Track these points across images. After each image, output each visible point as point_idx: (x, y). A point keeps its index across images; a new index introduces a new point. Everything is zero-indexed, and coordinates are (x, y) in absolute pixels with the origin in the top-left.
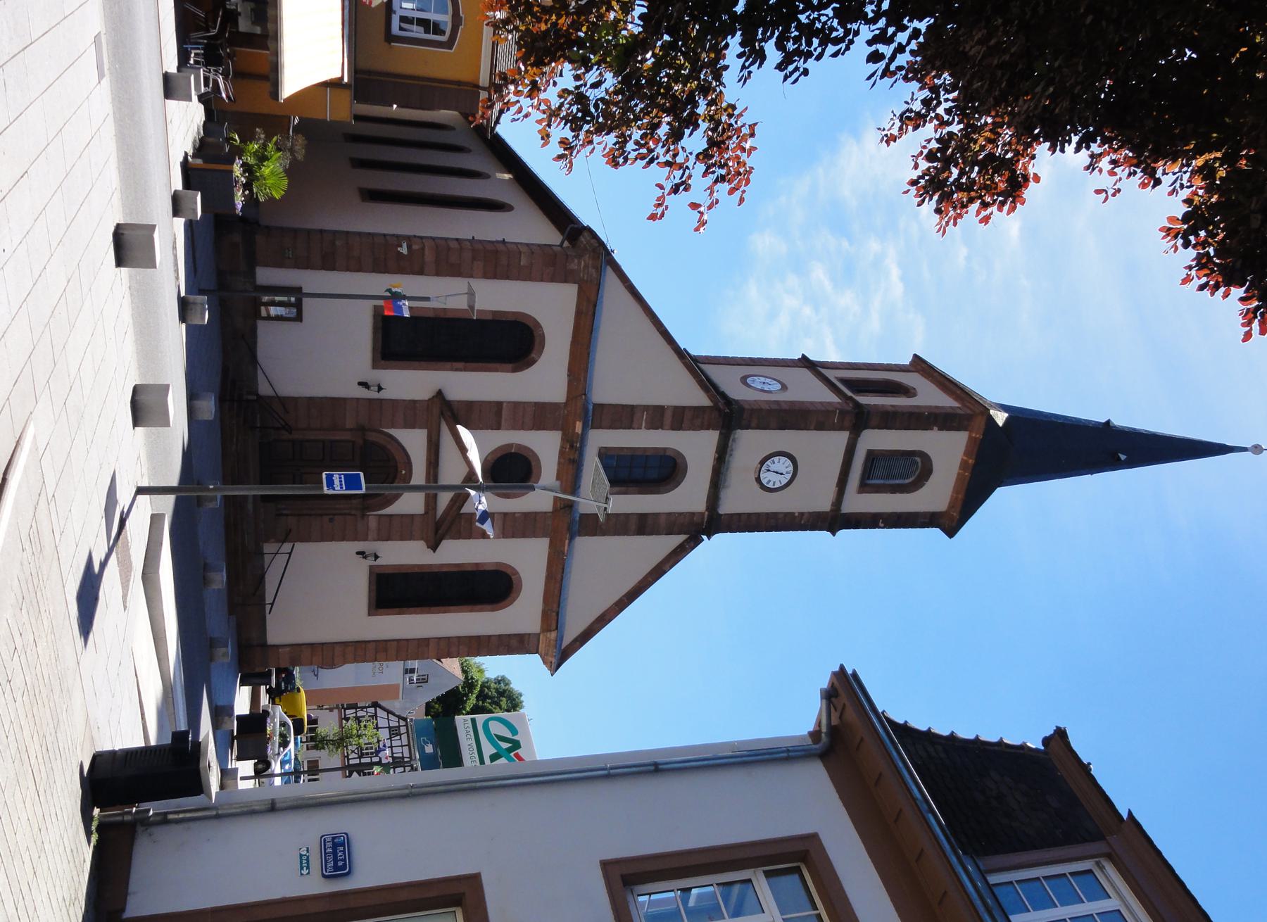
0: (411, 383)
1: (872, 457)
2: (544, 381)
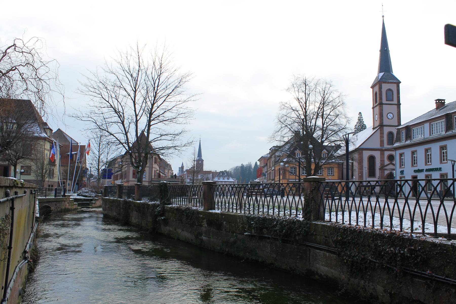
1: (387, 100)
2: (377, 155)
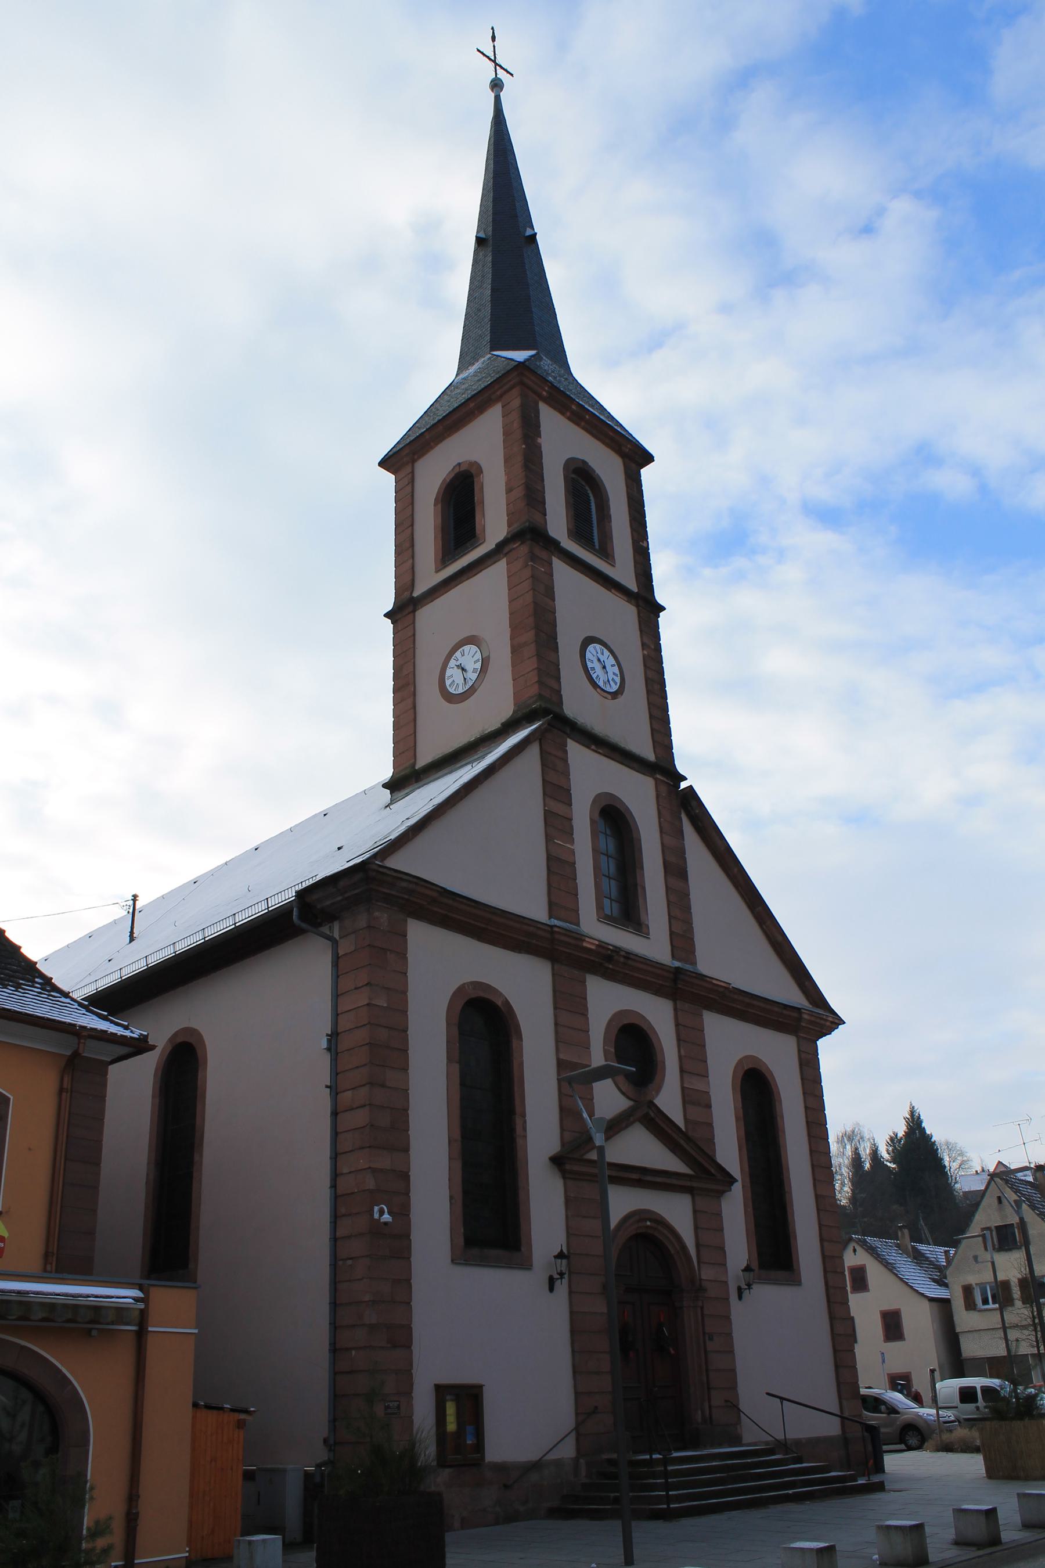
0: (546, 1208)
2: (525, 986)
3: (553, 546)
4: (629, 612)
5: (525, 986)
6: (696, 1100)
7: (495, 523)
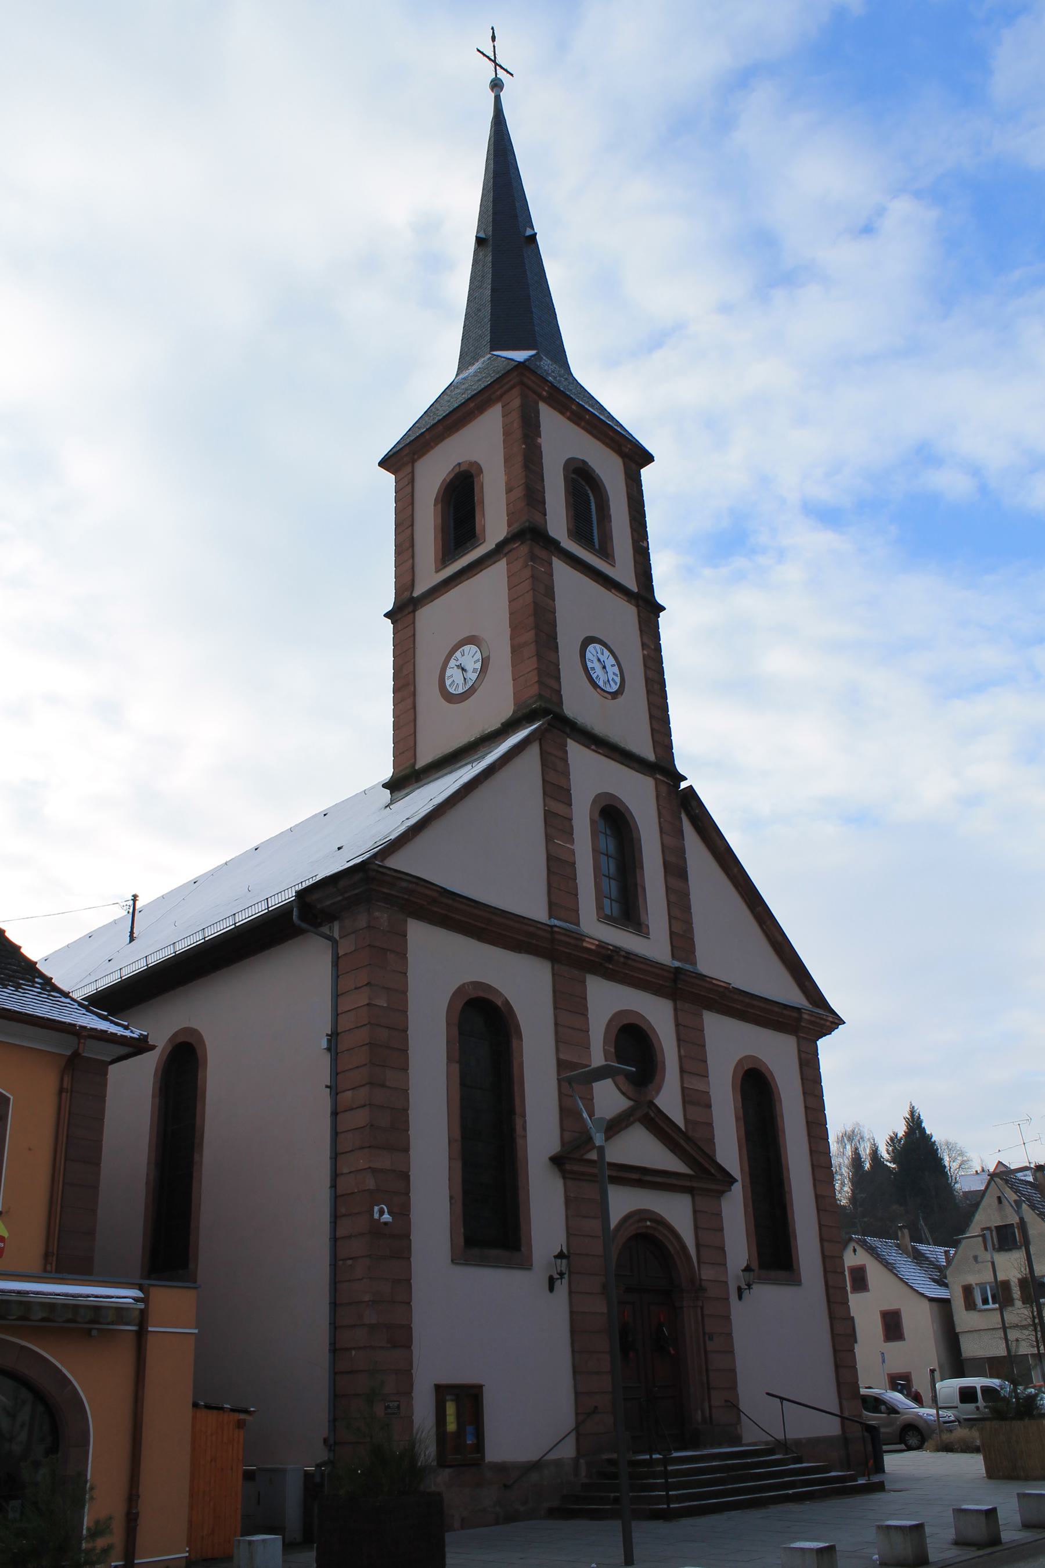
0: (546, 1208)
2: (525, 986)
3: (553, 546)
4: (629, 612)
5: (525, 986)
6: (696, 1100)
7: (495, 523)
